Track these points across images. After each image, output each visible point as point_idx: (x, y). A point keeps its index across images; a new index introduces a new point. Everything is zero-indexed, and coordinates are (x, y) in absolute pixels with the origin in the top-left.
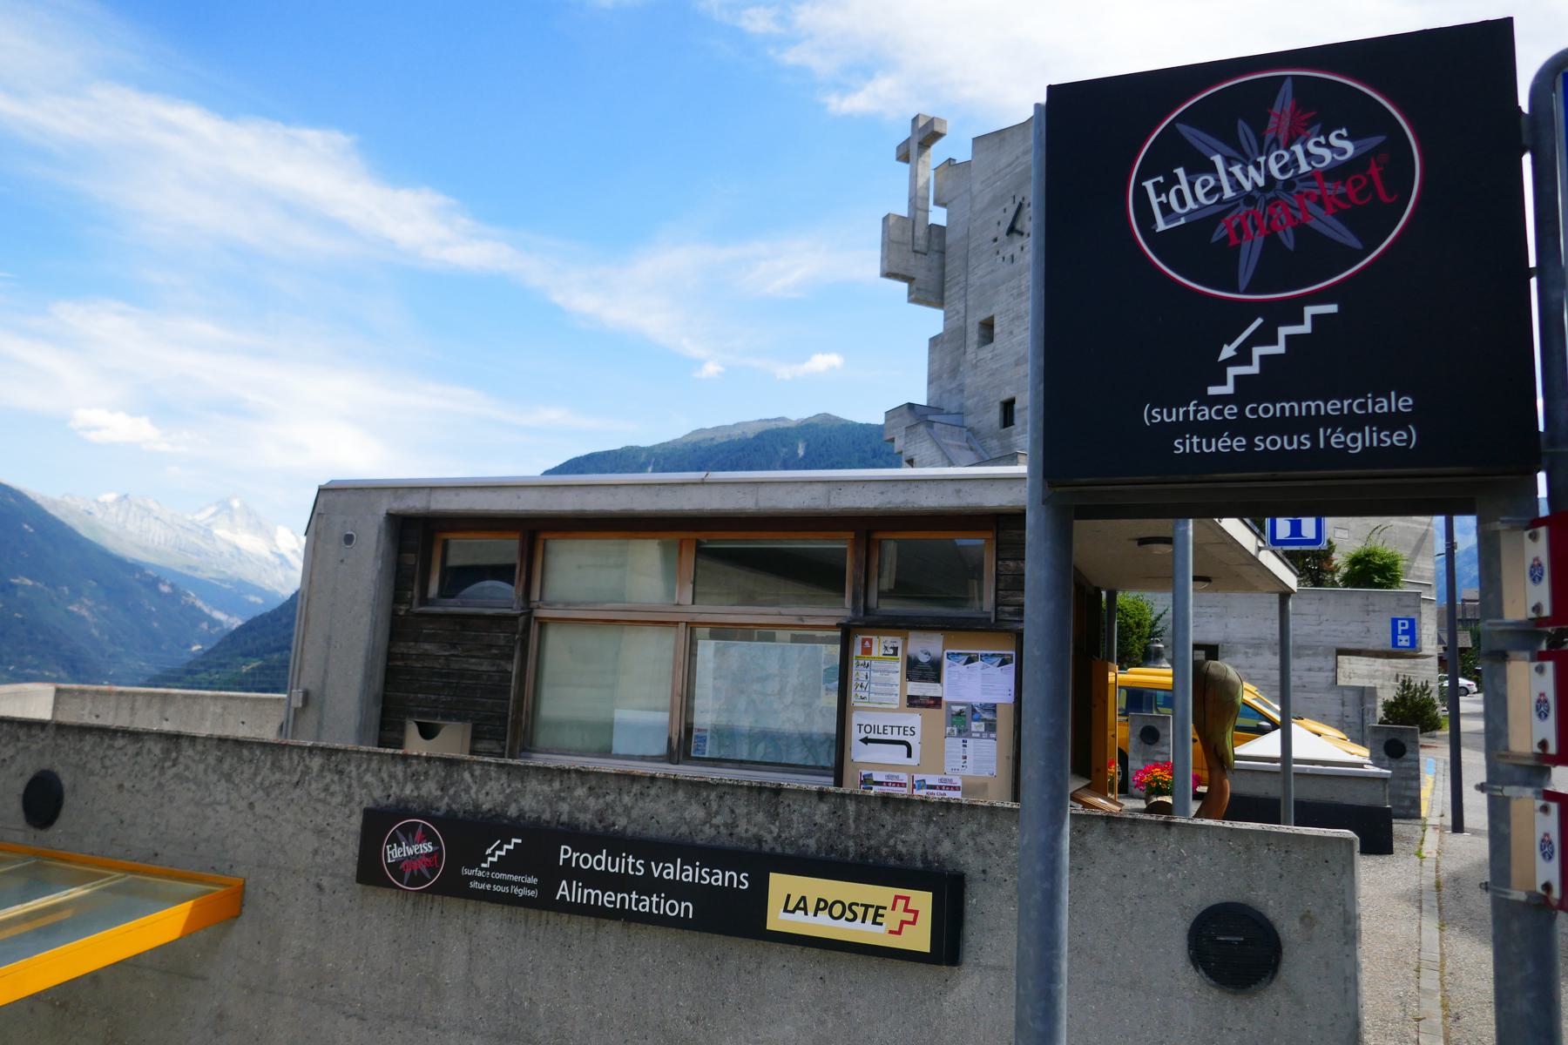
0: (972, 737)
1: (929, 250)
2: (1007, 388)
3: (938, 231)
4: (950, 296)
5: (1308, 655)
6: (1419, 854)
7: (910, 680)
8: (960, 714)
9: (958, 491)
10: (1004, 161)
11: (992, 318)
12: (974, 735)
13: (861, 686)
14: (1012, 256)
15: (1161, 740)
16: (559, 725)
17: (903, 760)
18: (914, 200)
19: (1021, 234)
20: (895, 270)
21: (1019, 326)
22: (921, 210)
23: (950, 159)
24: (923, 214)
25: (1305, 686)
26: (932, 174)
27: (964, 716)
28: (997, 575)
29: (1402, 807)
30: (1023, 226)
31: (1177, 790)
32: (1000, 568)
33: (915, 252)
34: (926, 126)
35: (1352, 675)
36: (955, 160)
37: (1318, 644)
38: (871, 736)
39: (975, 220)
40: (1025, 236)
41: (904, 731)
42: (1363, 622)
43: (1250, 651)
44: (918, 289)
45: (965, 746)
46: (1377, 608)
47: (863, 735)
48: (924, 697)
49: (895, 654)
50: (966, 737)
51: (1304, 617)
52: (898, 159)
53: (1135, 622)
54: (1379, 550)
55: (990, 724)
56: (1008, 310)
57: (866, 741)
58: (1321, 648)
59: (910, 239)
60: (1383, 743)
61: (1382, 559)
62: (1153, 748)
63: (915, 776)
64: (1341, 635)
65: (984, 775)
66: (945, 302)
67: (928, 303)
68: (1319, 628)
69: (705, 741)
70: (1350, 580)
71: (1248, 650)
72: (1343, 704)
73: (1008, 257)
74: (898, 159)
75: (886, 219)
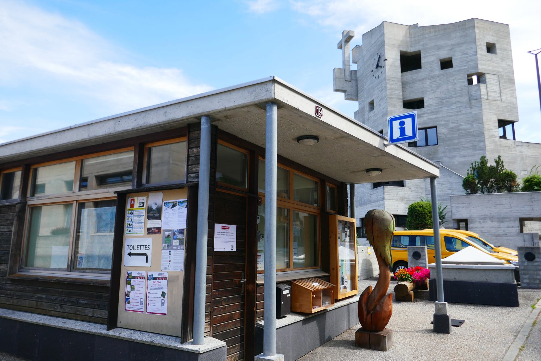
0: (173, 249)
1: (351, 80)
2: (380, 126)
3: (355, 72)
4: (360, 96)
5: (507, 221)
6: (533, 307)
7: (149, 219)
8: (168, 236)
9: (166, 113)
10: (373, 42)
11: (373, 101)
12: (174, 248)
13: (130, 225)
14: (379, 76)
15: (421, 257)
16: (374, 268)
17: (145, 264)
18: (344, 62)
19: (381, 67)
20: (338, 88)
21: (383, 102)
22: (347, 65)
23: (357, 45)
24: (348, 67)
25: (506, 234)
26: (351, 52)
27: (171, 237)
28: (188, 157)
29: (536, 284)
30: (382, 64)
31: (265, 273)
32: (190, 153)
33: (346, 81)
34: (347, 34)
35: (532, 230)
36: (359, 46)
37: (511, 216)
38: (132, 252)
39: (365, 65)
40: (382, 67)
41: (145, 248)
42: (530, 206)
43: (482, 221)
44: (348, 94)
45: (170, 254)
46: (536, 200)
47: (129, 251)
48: (154, 228)
49: (143, 206)
50: (171, 249)
51: (504, 205)
52: (338, 48)
53: (428, 211)
54: (536, 176)
55: (181, 241)
56: (378, 96)
57: (130, 254)
58: (512, 218)
59: (344, 76)
60: (524, 254)
61: (538, 179)
62: (419, 261)
63: (149, 272)
64: (521, 212)
65: (177, 271)
66: (359, 98)
67: (353, 100)
68: (511, 209)
69: (82, 259)
70: (525, 189)
71: (480, 221)
72: (524, 241)
73: (377, 76)
74: (338, 48)
75: (334, 70)
